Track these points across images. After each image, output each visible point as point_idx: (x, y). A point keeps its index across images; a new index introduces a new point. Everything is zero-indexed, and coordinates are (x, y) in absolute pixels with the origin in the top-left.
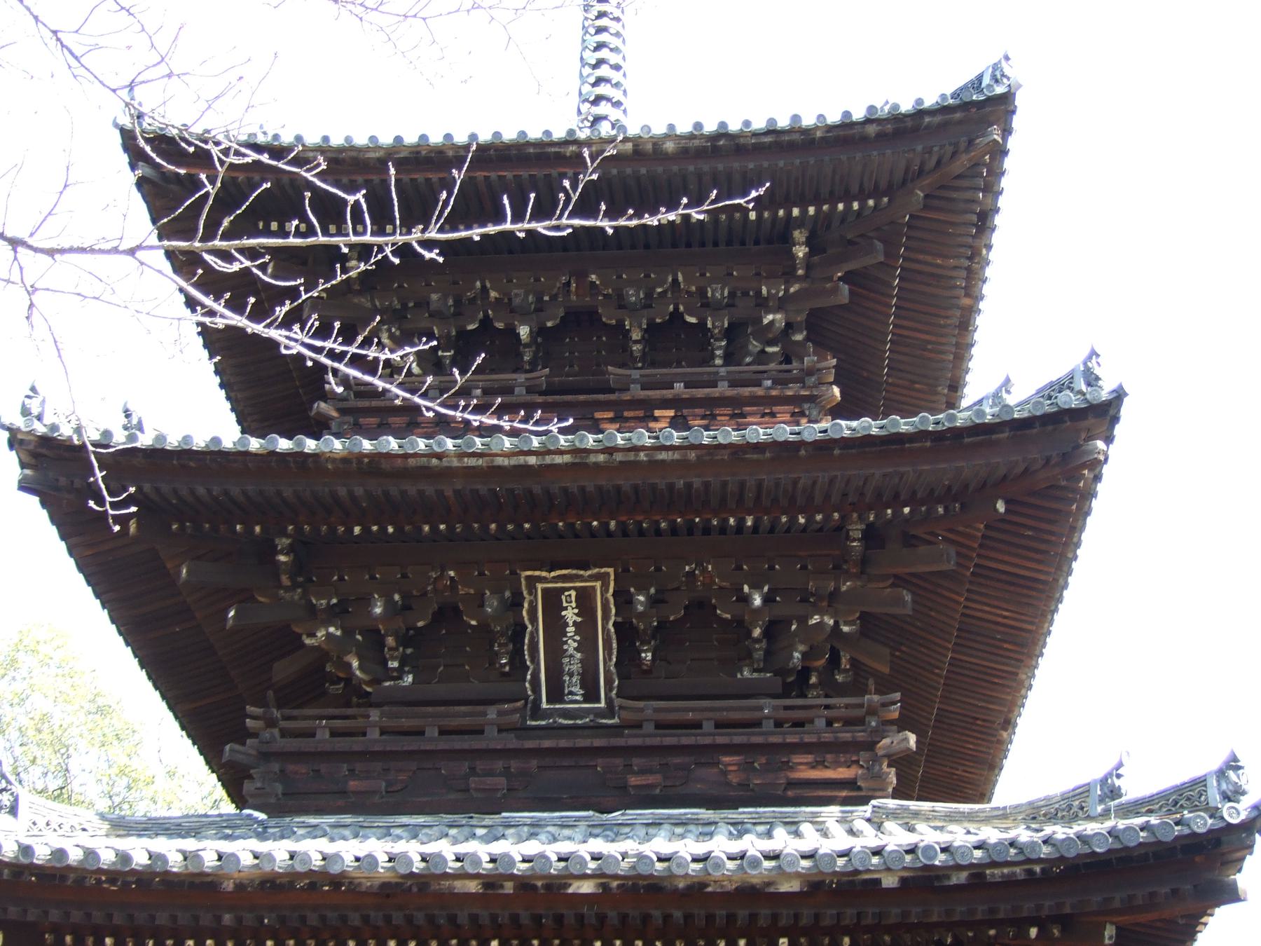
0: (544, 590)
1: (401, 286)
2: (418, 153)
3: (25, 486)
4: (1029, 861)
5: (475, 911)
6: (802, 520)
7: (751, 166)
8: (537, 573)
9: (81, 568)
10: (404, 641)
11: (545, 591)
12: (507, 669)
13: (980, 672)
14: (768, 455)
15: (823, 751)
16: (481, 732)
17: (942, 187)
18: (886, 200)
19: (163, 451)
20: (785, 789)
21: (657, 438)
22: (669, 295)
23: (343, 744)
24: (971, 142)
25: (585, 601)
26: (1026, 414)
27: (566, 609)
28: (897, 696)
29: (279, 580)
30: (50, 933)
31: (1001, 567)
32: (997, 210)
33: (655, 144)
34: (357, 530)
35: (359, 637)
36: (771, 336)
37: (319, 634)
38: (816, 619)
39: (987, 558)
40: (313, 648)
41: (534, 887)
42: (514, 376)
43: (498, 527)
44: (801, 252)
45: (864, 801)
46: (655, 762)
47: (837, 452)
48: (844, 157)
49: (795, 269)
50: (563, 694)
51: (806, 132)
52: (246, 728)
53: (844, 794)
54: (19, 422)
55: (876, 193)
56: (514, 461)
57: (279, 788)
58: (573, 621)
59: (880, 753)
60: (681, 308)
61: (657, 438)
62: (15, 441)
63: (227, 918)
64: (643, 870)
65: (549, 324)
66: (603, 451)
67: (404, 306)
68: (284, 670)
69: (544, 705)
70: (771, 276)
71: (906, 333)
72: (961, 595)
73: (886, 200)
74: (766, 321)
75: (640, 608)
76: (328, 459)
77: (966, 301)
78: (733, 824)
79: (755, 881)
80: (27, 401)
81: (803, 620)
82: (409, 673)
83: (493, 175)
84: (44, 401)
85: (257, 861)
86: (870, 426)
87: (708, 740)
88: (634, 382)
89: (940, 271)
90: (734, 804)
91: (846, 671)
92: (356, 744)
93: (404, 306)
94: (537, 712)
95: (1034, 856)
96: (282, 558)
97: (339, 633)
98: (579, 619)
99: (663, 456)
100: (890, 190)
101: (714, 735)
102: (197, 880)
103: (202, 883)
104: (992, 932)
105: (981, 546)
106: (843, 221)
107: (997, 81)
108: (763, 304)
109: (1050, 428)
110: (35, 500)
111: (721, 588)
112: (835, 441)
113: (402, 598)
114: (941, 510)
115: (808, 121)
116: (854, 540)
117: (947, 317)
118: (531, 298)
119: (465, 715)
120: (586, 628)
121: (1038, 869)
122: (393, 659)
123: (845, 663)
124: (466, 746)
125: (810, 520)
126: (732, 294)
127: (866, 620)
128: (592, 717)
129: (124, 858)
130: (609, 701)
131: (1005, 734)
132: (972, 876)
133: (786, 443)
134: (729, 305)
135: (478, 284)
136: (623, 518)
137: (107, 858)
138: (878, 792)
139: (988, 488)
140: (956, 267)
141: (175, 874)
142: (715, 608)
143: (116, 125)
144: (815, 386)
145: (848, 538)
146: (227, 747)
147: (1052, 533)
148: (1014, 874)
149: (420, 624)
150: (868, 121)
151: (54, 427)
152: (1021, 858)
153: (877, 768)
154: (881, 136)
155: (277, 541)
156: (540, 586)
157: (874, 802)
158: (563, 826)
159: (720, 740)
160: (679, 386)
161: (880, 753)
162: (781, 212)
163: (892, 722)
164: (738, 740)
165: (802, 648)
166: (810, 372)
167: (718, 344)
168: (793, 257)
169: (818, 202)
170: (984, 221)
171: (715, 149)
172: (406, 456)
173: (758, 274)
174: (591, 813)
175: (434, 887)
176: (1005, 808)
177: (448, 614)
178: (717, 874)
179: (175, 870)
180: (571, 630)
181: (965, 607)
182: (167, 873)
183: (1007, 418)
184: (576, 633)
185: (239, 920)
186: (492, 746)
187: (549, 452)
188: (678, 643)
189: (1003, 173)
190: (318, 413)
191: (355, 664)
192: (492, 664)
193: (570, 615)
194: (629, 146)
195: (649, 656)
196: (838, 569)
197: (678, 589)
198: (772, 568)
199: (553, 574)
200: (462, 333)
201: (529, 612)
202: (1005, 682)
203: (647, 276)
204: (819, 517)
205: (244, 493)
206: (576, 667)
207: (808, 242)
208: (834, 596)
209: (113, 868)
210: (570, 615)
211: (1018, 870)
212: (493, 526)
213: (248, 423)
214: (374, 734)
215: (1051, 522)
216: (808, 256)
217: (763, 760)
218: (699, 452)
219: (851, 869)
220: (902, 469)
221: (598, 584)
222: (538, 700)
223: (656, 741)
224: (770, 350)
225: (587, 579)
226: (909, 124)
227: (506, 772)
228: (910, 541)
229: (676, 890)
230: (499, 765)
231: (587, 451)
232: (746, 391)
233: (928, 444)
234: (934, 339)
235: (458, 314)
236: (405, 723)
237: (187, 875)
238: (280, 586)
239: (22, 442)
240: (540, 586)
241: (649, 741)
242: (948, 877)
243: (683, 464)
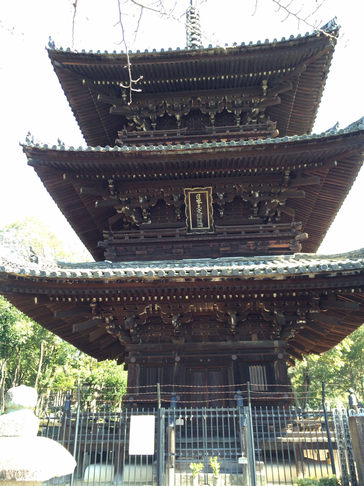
0: (191, 194)
1: (139, 103)
2: (145, 56)
3: (29, 164)
4: (356, 269)
5: (183, 287)
6: (272, 170)
7: (252, 57)
8: (189, 189)
9: (48, 190)
10: (148, 211)
11: (191, 194)
12: (180, 218)
13: (318, 216)
14: (264, 148)
15: (278, 239)
16: (175, 236)
17: (312, 63)
18: (294, 68)
19: (73, 151)
20: (268, 251)
21: (229, 144)
22: (223, 104)
23: (133, 241)
24: (324, 47)
25: (203, 197)
26: (347, 132)
27: (197, 199)
28: (301, 222)
29: (110, 193)
30: (51, 297)
31: (331, 183)
32: (329, 71)
33: (221, 51)
34: (134, 176)
35: (134, 210)
36: (254, 116)
37: (123, 209)
38: (274, 201)
39: (328, 181)
40: (120, 214)
41: (201, 280)
42: (176, 130)
43: (178, 174)
44: (265, 88)
45: (292, 254)
46: (228, 244)
47: (286, 146)
48: (282, 53)
49: (263, 93)
50: (197, 225)
51: (270, 45)
52: (103, 237)
53: (285, 252)
54: (26, 143)
55: (291, 67)
56: (184, 152)
57: (115, 254)
58: (200, 203)
59: (297, 239)
60: (226, 108)
61: (229, 144)
62: (25, 150)
63: (107, 291)
64: (235, 274)
65: (185, 114)
66: (211, 148)
67: (140, 109)
68: (112, 220)
69: (191, 229)
70: (255, 96)
71: (296, 114)
72: (317, 192)
73: (294, 68)
74: (253, 111)
75: (221, 198)
76: (125, 153)
77: (315, 103)
78: (253, 261)
79: (269, 276)
80: (28, 137)
81: (269, 201)
82: (150, 220)
83: (169, 63)
84: (33, 137)
85: (115, 274)
86: (297, 138)
87: (244, 237)
88: (214, 131)
89: (308, 93)
90: (253, 255)
91: (279, 217)
92: (138, 241)
93: (140, 109)
94: (189, 230)
95: (358, 268)
96: (111, 186)
97: (128, 209)
98: (201, 203)
99: (231, 149)
100: (295, 65)
101: (245, 235)
102: (97, 280)
103: (99, 281)
104: (340, 291)
105: (327, 177)
106: (279, 76)
107: (333, 26)
108: (252, 105)
109: (355, 136)
110: (32, 168)
111: (244, 192)
112: (286, 143)
113: (147, 198)
114: (316, 165)
115: (271, 41)
116: (287, 176)
117: (310, 108)
118: (180, 106)
119: (169, 231)
120: (204, 205)
121: (359, 271)
122: (145, 216)
123: (279, 215)
124: (171, 240)
125: (275, 169)
126: (242, 103)
127: (289, 203)
128: (206, 231)
129: (75, 274)
130: (211, 227)
131: (323, 235)
132: (338, 274)
133: (270, 144)
134: (241, 107)
135: (163, 101)
136: (216, 171)
137: (58, 274)
138: (297, 251)
139: (332, 157)
140: (314, 91)
141: (90, 279)
142: (242, 198)
143: (46, 48)
144: (271, 130)
145: (284, 175)
146: (99, 242)
147: (351, 171)
148: (351, 273)
149: (153, 205)
150: (290, 40)
151: (37, 145)
152: (354, 268)
153: (296, 244)
154: (294, 46)
155: (109, 181)
156: (189, 193)
157: (295, 254)
158: (201, 263)
159: (247, 237)
160: (228, 132)
161: (297, 239)
162: (260, 74)
163: (299, 230)
164: (253, 237)
165: (269, 210)
166: (269, 126)
167: (238, 119)
168: (262, 89)
169: (272, 70)
170: (324, 76)
171: (240, 52)
172: (150, 152)
173: (251, 96)
174: (210, 259)
175: (170, 280)
176: (340, 254)
177: (161, 202)
178: (258, 275)
179: (90, 277)
180: (199, 206)
181: (318, 197)
182: (88, 278)
183: (342, 134)
184: (200, 207)
185: (111, 292)
186: (178, 240)
187: (195, 149)
188: (232, 208)
189: (332, 58)
190: (117, 142)
191: (134, 218)
192: (175, 217)
193: (199, 201)
194: (213, 51)
195: (222, 213)
196: (281, 185)
197: (231, 193)
198: (260, 186)
199: (193, 189)
200: (159, 118)
201: (186, 201)
202: (327, 219)
203: (216, 98)
204: (278, 168)
205: (99, 165)
206: (201, 217)
207: (267, 84)
208: (280, 194)
209: (71, 277)
210: (199, 201)
211: (352, 272)
212: (176, 174)
213: (89, 143)
214: (142, 238)
215: (351, 168)
216: (267, 89)
217: (261, 242)
218: (242, 148)
219: (299, 272)
220: (307, 151)
221: (207, 192)
222: (189, 227)
223: (228, 237)
224: (253, 121)
225: (204, 190)
226: (304, 41)
227: (183, 247)
228: (304, 176)
229: (245, 280)
230: (181, 246)
231: (207, 149)
232: (249, 132)
233: (315, 143)
234: (304, 116)
235: (157, 112)
236: (151, 234)
237: (93, 279)
238: (110, 195)
239: (27, 150)
240: (189, 193)
241: (226, 238)
242: (330, 274)
243: (237, 152)
